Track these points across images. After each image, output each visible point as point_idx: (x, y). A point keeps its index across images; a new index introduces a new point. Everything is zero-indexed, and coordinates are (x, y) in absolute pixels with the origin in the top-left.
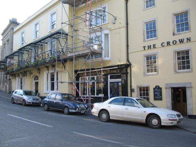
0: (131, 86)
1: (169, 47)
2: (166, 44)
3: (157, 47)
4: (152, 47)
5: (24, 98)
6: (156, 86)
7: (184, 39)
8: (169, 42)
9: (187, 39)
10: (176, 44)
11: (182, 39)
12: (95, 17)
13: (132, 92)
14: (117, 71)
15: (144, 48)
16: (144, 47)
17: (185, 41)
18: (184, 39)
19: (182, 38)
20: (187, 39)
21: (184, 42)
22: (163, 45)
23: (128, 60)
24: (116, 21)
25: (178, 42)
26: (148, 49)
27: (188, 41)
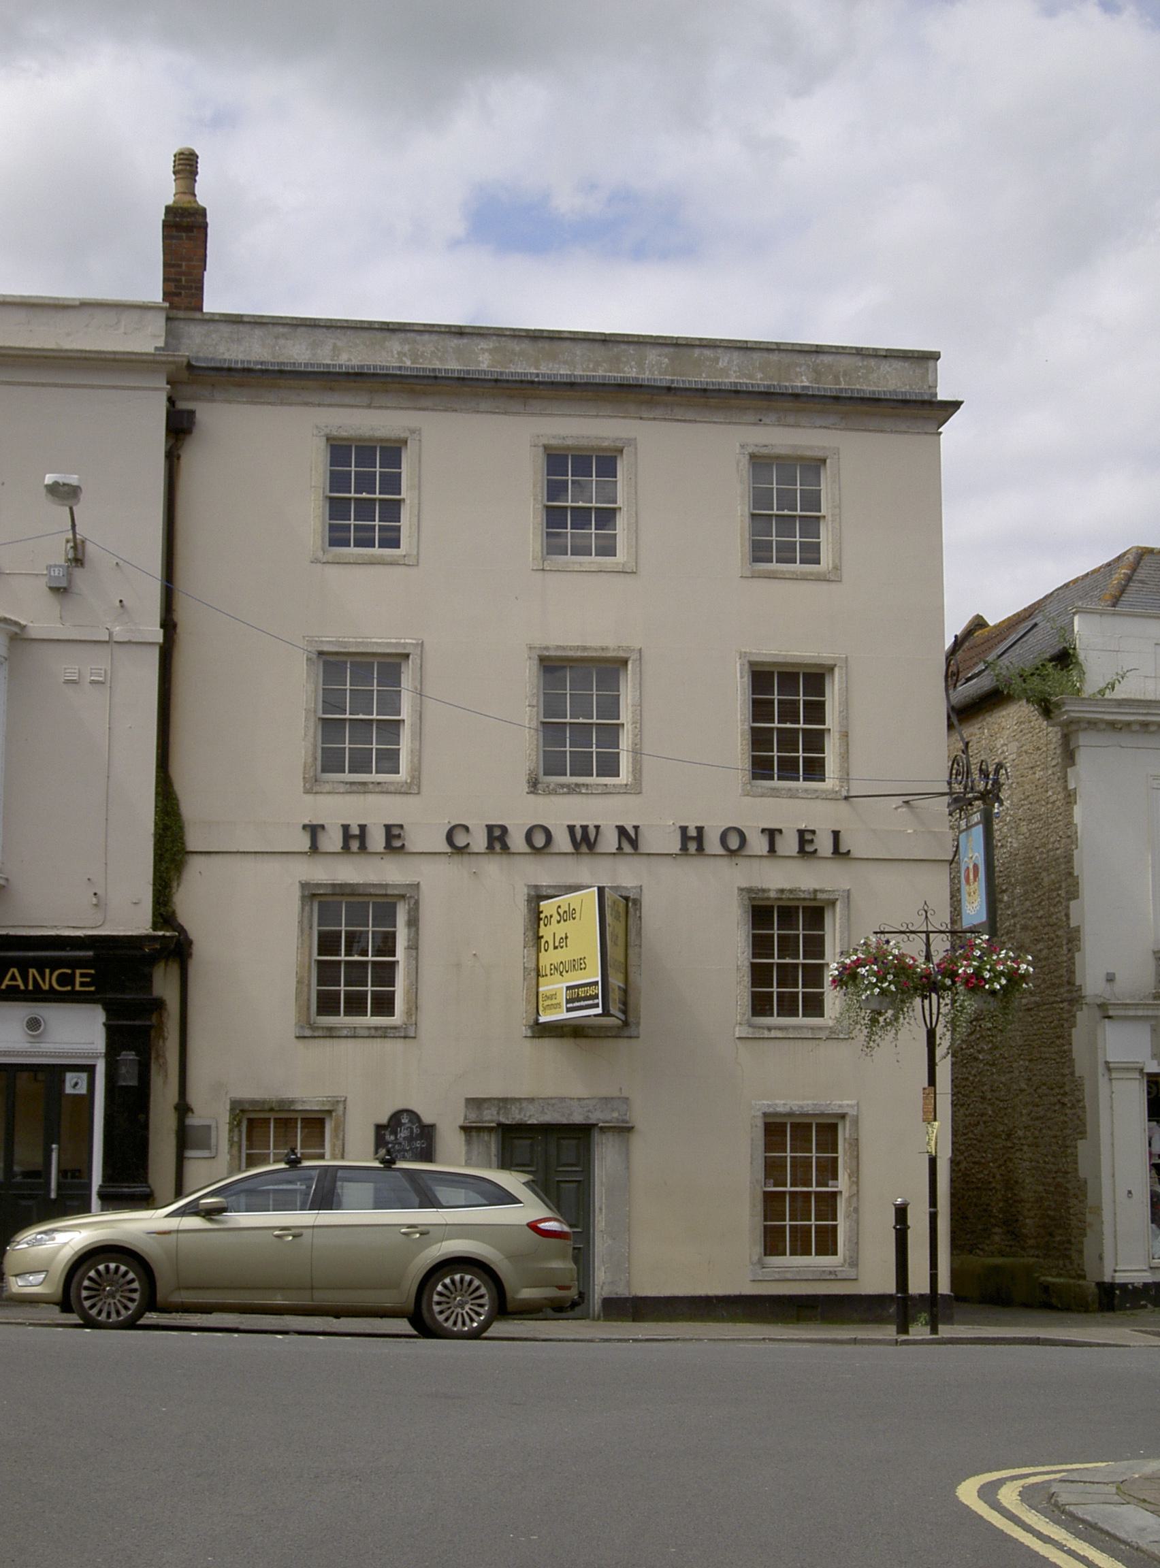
0: (183, 1109)
1: (493, 867)
2: (479, 841)
3: (411, 847)
4: (377, 840)
5: (811, 889)
6: (396, 1117)
7: (597, 827)
8: (504, 829)
9: (622, 831)
10: (546, 851)
11: (585, 828)
12: (963, 813)
13: (190, 1153)
14: (65, 980)
15: (843, 849)
16: (314, 831)
17: (609, 841)
18: (597, 827)
19: (591, 823)
20: (622, 831)
21: (601, 848)
22: (460, 840)
23: (164, 912)
24: (78, 572)
25: (562, 842)
26: (346, 847)
27: (627, 848)
